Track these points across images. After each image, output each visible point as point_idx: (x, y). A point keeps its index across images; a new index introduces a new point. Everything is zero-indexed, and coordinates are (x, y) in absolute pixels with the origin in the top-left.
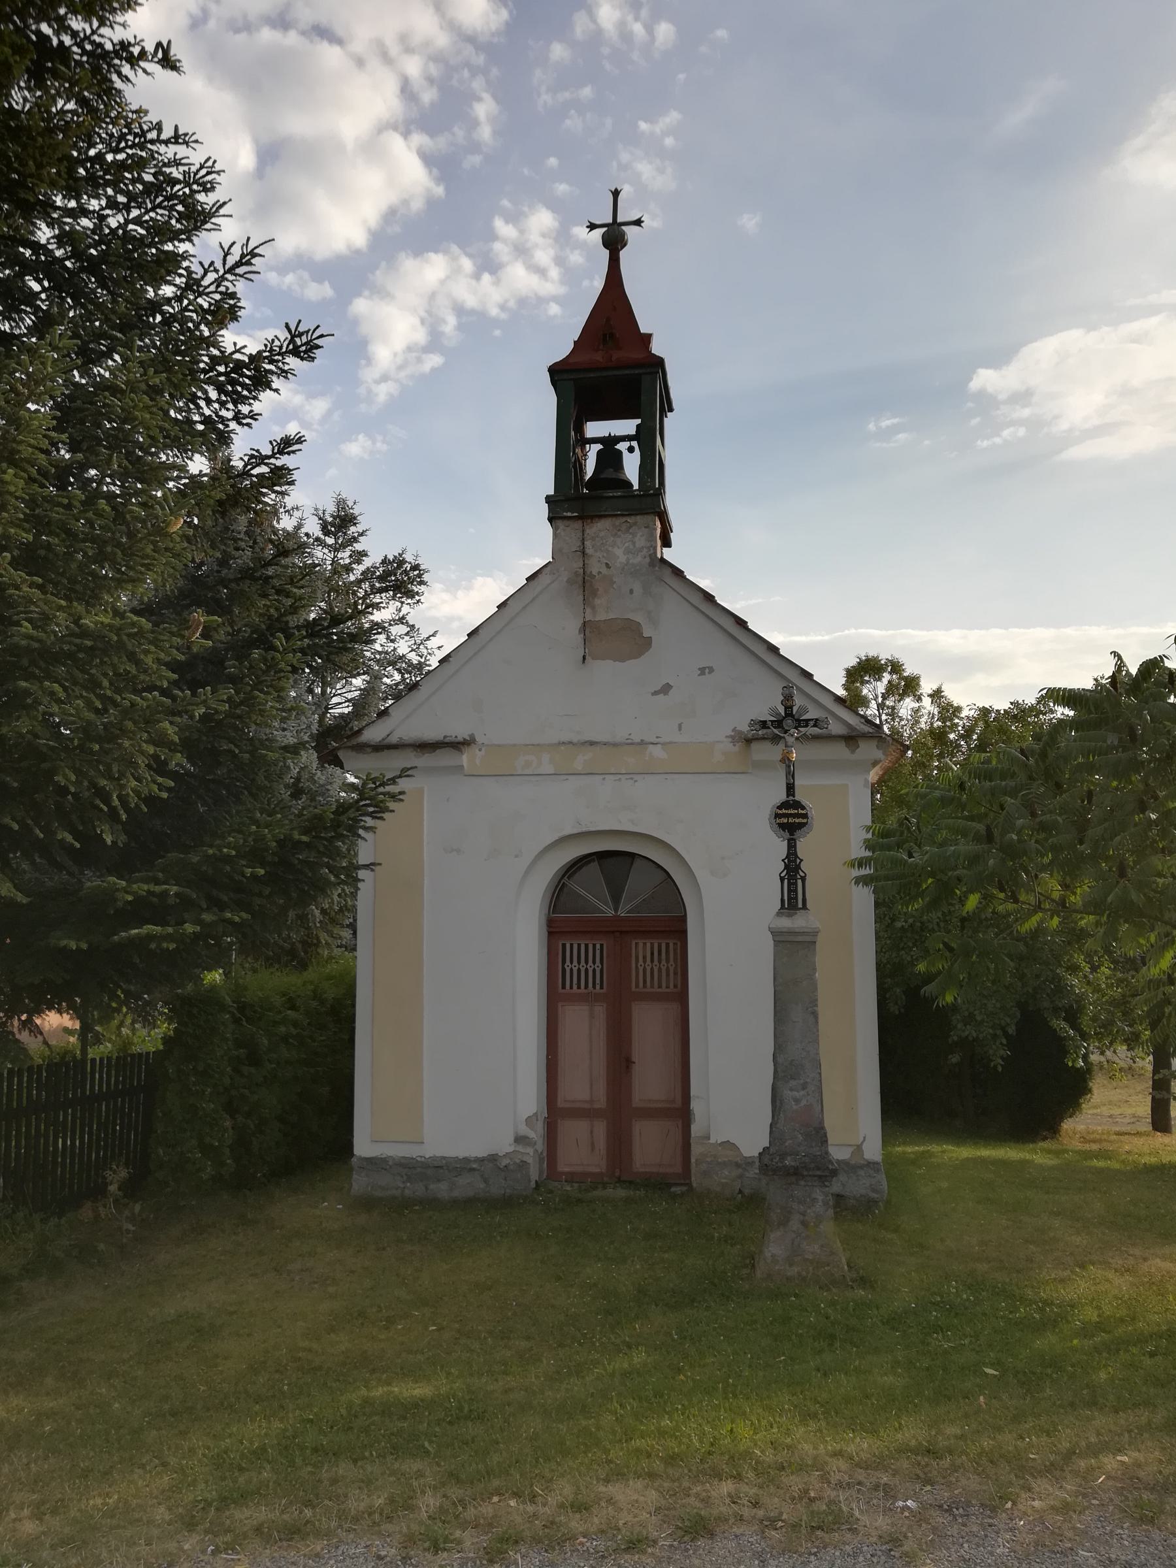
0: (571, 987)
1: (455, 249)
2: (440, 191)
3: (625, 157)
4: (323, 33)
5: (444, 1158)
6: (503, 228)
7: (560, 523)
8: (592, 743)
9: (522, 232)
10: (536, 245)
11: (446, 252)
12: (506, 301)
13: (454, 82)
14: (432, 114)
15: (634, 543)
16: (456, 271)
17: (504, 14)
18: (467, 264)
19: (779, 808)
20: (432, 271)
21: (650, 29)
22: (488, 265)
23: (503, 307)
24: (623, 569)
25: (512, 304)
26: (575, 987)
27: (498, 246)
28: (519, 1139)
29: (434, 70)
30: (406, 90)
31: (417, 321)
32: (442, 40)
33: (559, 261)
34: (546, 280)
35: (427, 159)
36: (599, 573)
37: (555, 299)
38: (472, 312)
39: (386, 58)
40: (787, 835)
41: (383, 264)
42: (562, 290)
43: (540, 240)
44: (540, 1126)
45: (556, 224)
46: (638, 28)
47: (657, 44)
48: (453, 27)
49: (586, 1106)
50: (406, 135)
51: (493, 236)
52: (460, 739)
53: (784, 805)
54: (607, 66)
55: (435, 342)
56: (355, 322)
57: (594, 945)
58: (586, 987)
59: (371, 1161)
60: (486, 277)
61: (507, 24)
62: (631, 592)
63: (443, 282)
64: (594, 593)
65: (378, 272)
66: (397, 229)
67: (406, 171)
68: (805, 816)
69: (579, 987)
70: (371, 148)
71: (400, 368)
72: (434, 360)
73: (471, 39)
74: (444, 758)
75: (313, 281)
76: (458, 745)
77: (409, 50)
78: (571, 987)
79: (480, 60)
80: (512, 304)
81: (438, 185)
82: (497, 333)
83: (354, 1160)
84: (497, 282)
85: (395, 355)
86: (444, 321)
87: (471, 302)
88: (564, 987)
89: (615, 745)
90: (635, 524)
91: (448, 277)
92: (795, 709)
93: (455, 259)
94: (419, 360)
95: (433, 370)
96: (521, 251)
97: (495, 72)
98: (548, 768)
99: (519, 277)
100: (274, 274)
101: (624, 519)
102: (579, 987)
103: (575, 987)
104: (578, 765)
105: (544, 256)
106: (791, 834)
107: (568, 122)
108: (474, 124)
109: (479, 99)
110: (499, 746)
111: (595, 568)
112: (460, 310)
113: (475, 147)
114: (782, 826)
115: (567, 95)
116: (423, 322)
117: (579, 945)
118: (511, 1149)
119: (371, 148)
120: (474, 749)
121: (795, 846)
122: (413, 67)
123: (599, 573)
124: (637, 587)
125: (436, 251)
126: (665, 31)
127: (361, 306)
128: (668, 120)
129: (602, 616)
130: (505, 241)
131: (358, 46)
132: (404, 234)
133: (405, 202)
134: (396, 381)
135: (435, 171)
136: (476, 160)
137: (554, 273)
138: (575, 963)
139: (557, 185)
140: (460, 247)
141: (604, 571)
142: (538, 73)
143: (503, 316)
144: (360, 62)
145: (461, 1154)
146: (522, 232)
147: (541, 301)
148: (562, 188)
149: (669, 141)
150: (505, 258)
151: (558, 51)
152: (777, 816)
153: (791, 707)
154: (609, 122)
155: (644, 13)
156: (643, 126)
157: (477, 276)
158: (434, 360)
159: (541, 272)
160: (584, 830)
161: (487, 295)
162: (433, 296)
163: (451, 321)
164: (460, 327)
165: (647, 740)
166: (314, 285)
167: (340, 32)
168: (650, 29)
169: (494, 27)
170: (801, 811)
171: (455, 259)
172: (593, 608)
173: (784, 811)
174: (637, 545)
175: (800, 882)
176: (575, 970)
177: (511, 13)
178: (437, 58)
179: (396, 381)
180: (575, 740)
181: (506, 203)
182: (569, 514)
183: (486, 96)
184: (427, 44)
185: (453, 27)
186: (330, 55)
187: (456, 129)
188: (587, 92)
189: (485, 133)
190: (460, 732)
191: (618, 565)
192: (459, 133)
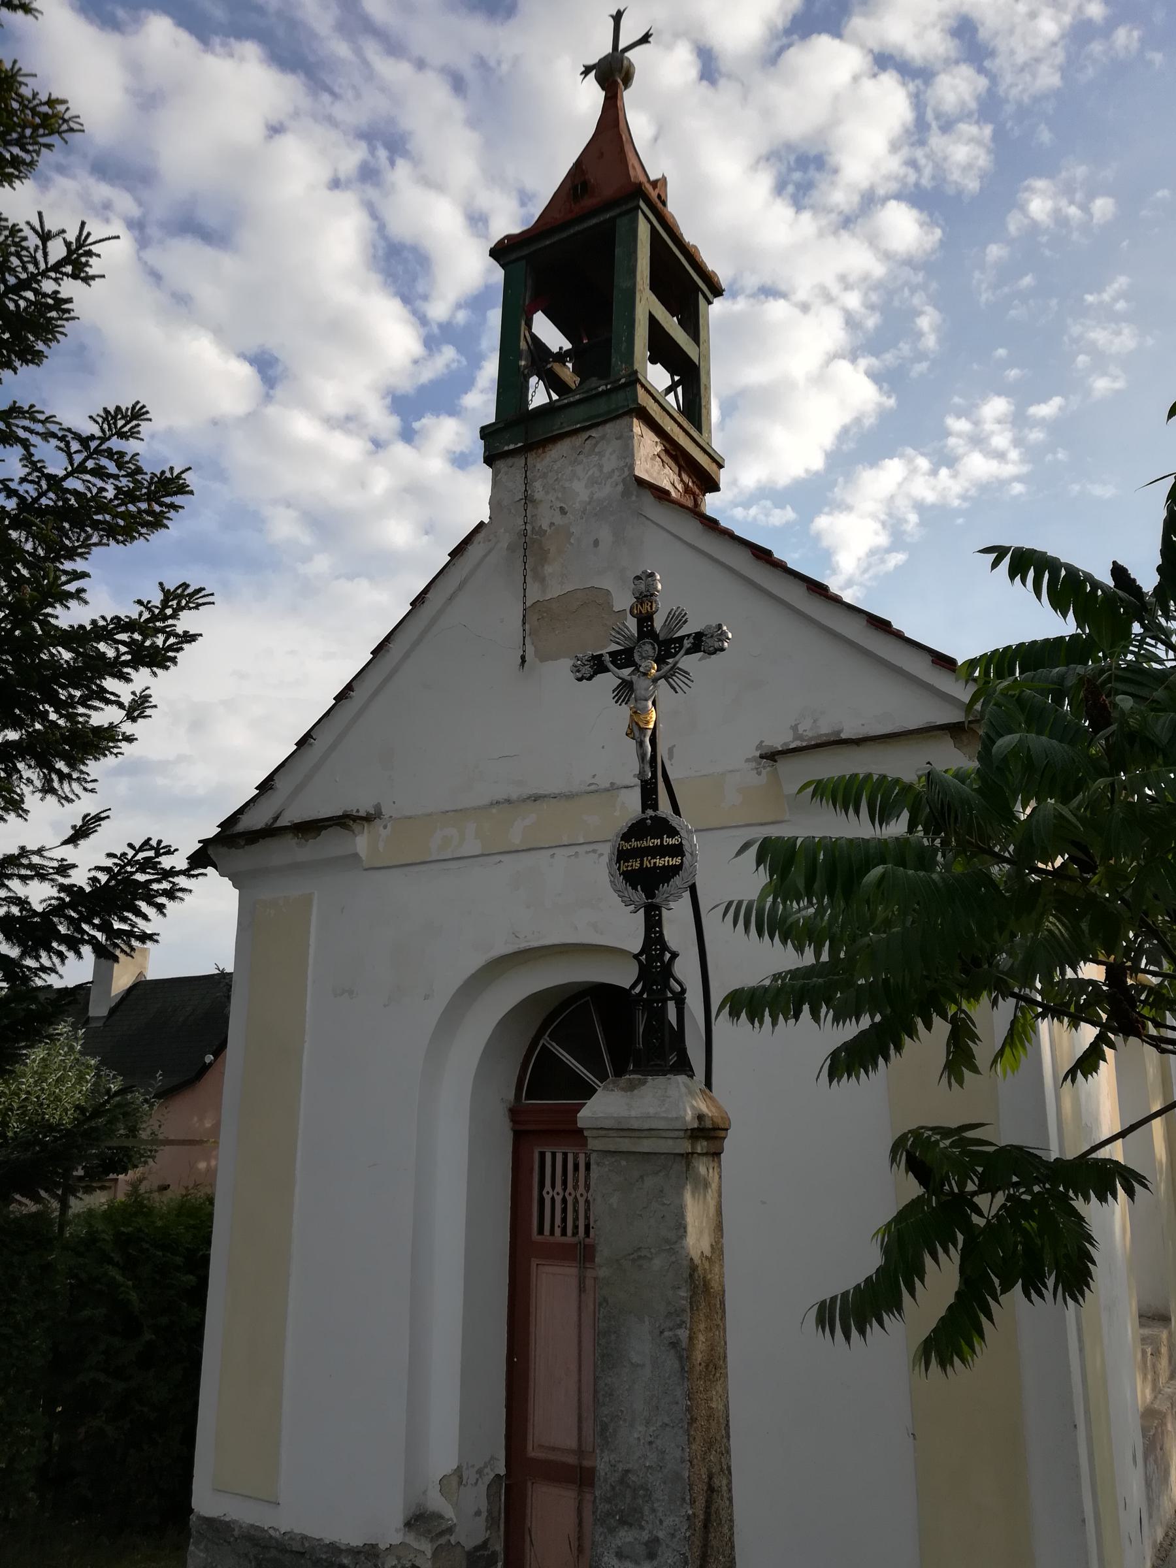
0: (552, 1233)
1: (910, 451)
2: (891, 402)
3: (1076, 330)
4: (769, 292)
5: (305, 1538)
6: (960, 425)
7: (500, 464)
8: (536, 798)
9: (976, 423)
10: (993, 433)
11: (901, 456)
12: (967, 490)
13: (896, 303)
14: (878, 337)
15: (600, 467)
16: (914, 471)
17: (938, 233)
18: (923, 463)
19: (626, 837)
20: (887, 478)
21: (1085, 208)
22: (946, 460)
23: (964, 497)
24: (584, 512)
25: (973, 492)
26: (558, 1231)
27: (952, 441)
28: (419, 1521)
29: (874, 297)
30: (851, 322)
31: (878, 526)
32: (878, 270)
33: (1017, 442)
34: (1007, 463)
35: (875, 377)
36: (552, 524)
37: (1017, 478)
38: (933, 506)
39: (829, 299)
40: (639, 896)
41: (841, 480)
42: (1024, 469)
43: (996, 427)
44: (476, 1498)
45: (1013, 408)
46: (1073, 211)
47: (1095, 221)
48: (887, 256)
49: (571, 1460)
50: (853, 360)
51: (948, 433)
52: (362, 813)
53: (636, 830)
54: (1047, 253)
55: (898, 539)
56: (818, 537)
57: (554, 1155)
58: (575, 1233)
59: (209, 1521)
60: (944, 472)
61: (941, 241)
62: (596, 543)
63: (900, 485)
64: (543, 557)
65: (836, 490)
66: (852, 445)
67: (858, 392)
68: (678, 850)
69: (564, 1233)
70: (821, 379)
71: (865, 571)
72: (897, 559)
73: (909, 262)
74: (331, 844)
75: (776, 507)
76: (345, 821)
77: (847, 287)
78: (552, 1233)
79: (920, 277)
80: (973, 492)
81: (889, 397)
82: (960, 521)
83: (193, 1518)
84: (955, 476)
85: (859, 559)
86: (906, 521)
87: (930, 497)
88: (541, 1231)
89: (569, 796)
90: (603, 437)
91: (905, 479)
92: (658, 623)
93: (910, 461)
94: (883, 561)
95: (897, 567)
96: (978, 441)
97: (934, 285)
98: (472, 847)
99: (978, 466)
100: (740, 509)
101: (585, 435)
102: (564, 1233)
103: (558, 1231)
104: (516, 839)
105: (1001, 440)
106: (650, 894)
107: (1013, 313)
108: (920, 335)
109: (920, 313)
110: (410, 818)
111: (546, 517)
112: (920, 507)
113: (920, 356)
114: (632, 879)
115: (1006, 290)
116: (884, 524)
117: (565, 1155)
118: (396, 1538)
119: (821, 379)
120: (381, 831)
121: (659, 923)
122: (853, 300)
123: (552, 524)
124: (605, 534)
125: (891, 458)
126: (1103, 207)
127: (822, 522)
128: (1116, 286)
129: (555, 590)
130: (959, 435)
131: (801, 295)
132: (859, 448)
133: (858, 421)
134: (861, 584)
135: (885, 385)
136: (922, 367)
137: (1014, 455)
138: (559, 1187)
139: (1007, 372)
140: (915, 449)
141: (558, 519)
142: (977, 275)
143: (966, 505)
144: (805, 308)
145: (329, 1536)
146: (976, 423)
147: (1002, 483)
148: (1013, 373)
149: (1121, 305)
150: (960, 451)
151: (995, 251)
152: (622, 856)
153: (649, 617)
154: (1054, 302)
155: (1079, 196)
156: (1090, 298)
157: (934, 472)
158: (897, 559)
159: (1001, 456)
160: (523, 945)
161: (944, 487)
162: (892, 498)
163: (913, 518)
164: (922, 523)
165: (619, 782)
166: (777, 511)
167: (783, 287)
168: (1085, 208)
169: (928, 247)
170: (668, 841)
171: (910, 461)
172: (542, 580)
173: (634, 844)
174: (605, 470)
175: (671, 1007)
176: (558, 1199)
177: (944, 232)
178: (878, 286)
179: (861, 584)
180: (514, 796)
181: (957, 400)
182: (512, 447)
183: (929, 309)
184: (865, 278)
185: (887, 256)
186: (777, 309)
187: (901, 345)
188: (1027, 280)
189: (930, 341)
190: (363, 805)
191: (577, 506)
192: (905, 348)
